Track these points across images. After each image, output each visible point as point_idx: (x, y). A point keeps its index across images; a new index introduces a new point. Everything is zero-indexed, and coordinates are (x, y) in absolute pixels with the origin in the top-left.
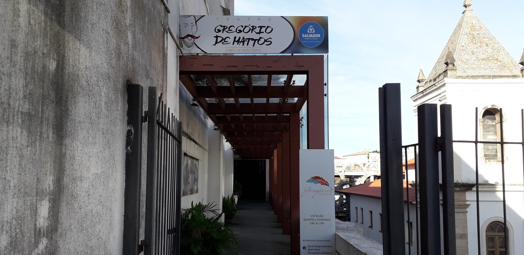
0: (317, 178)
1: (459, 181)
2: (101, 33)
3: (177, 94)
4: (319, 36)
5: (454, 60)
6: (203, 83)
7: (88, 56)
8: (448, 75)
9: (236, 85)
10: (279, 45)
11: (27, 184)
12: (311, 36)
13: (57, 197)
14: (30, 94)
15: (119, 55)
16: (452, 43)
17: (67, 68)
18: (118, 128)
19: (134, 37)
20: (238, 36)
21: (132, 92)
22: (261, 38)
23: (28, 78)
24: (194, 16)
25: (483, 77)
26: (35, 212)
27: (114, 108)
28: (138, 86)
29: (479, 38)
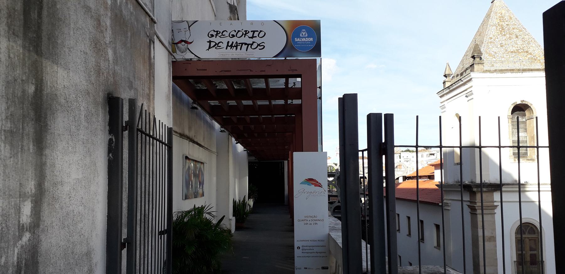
0: (310, 180)
1: (487, 181)
2: (79, 54)
3: (169, 100)
4: (311, 39)
5: (481, 54)
6: (201, 86)
7: (66, 77)
8: (475, 70)
9: (235, 87)
10: (272, 48)
11: (11, 188)
12: (304, 40)
13: (38, 200)
14: (11, 115)
15: (98, 72)
16: (479, 35)
17: (45, 90)
18: (99, 137)
19: (115, 53)
20: (231, 40)
21: (112, 103)
22: (254, 42)
23: (9, 102)
24: (187, 22)
25: (512, 71)
26: (18, 211)
27: (94, 120)
28: (118, 99)
29: (509, 29)
